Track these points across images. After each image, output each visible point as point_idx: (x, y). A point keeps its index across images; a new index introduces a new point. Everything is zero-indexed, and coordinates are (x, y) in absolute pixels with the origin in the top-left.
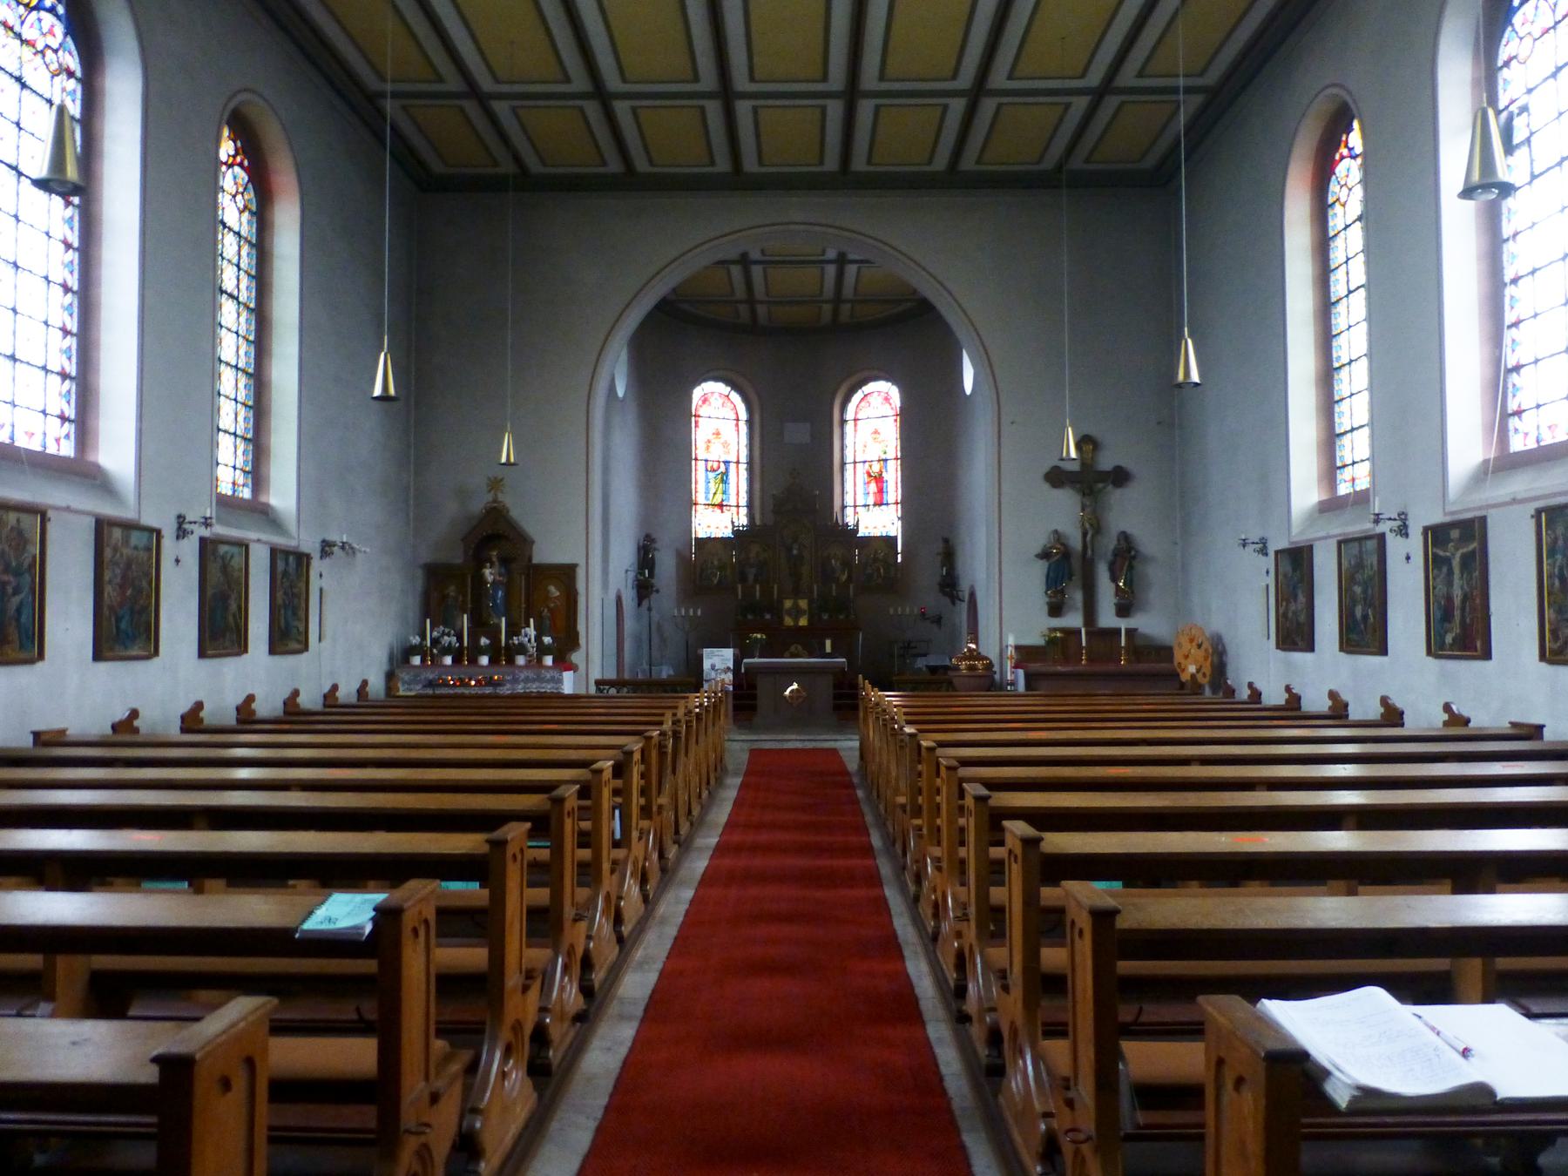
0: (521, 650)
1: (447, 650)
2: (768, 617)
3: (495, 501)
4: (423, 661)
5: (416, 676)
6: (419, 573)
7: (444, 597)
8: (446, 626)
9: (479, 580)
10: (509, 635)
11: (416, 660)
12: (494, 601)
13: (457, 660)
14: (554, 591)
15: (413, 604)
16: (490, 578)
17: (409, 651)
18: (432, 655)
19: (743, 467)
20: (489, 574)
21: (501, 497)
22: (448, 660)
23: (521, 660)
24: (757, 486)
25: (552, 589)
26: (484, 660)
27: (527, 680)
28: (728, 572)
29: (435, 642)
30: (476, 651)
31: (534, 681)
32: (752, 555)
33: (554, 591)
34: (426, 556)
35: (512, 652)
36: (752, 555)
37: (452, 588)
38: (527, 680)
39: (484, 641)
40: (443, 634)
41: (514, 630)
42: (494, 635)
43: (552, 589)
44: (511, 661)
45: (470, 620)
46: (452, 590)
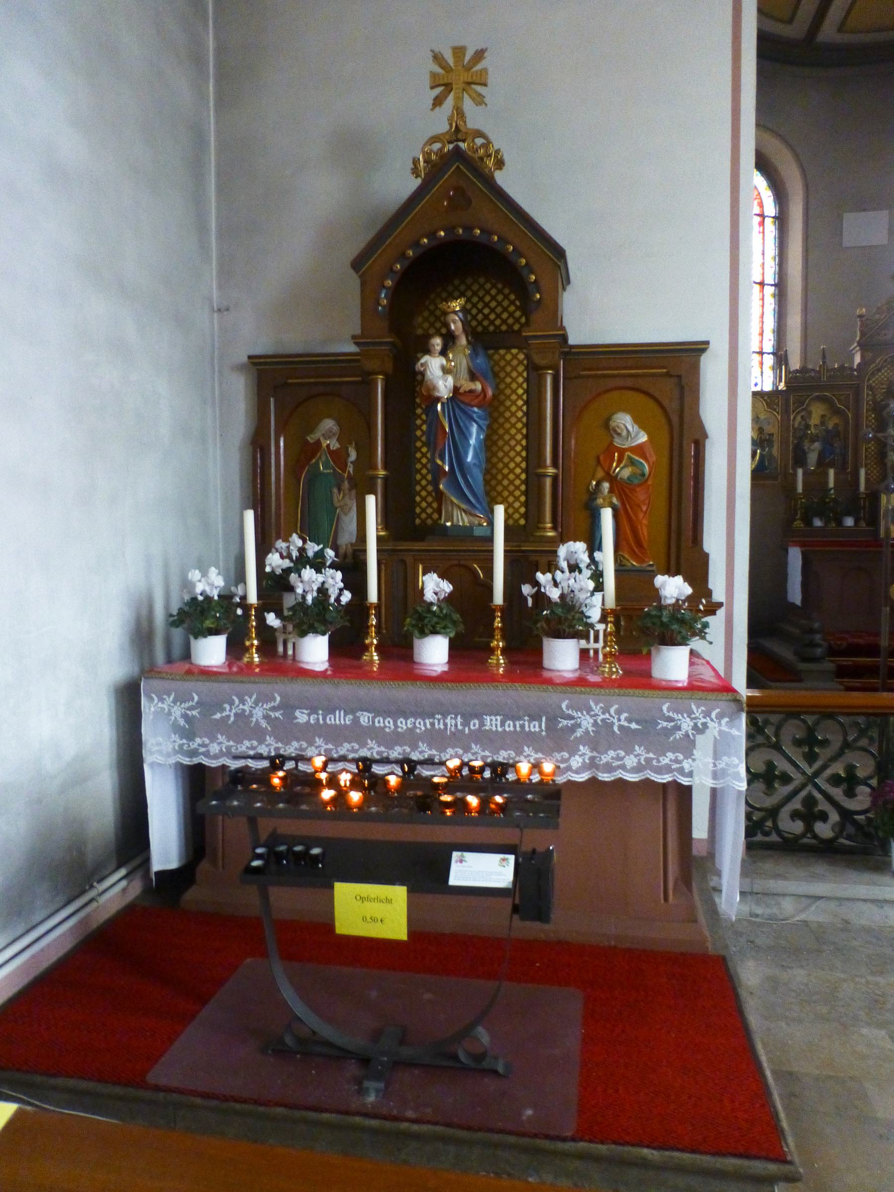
0: (567, 620)
1: (309, 618)
2: (849, 522)
3: (457, 133)
4: (235, 648)
5: (209, 706)
6: (239, 390)
7: (304, 454)
8: (309, 532)
9: (408, 385)
10: (522, 566)
11: (212, 651)
12: (459, 458)
13: (346, 649)
14: (630, 430)
15: (222, 467)
16: (444, 386)
17: (197, 616)
18: (264, 631)
19: (769, 291)
20: (440, 373)
21: (475, 118)
22: (315, 651)
23: (563, 656)
24: (795, 321)
25: (624, 421)
26: (434, 652)
27: (603, 736)
28: (775, 451)
29: (275, 586)
30: (406, 619)
31: (627, 740)
32: (815, 420)
33: (630, 430)
34: (258, 338)
35: (532, 625)
36: (815, 420)
37: (328, 424)
38: (603, 736)
39: (434, 586)
40: (302, 561)
41: (527, 561)
42: (464, 559)
43: (624, 421)
44: (527, 661)
45: (386, 517)
46: (327, 432)
